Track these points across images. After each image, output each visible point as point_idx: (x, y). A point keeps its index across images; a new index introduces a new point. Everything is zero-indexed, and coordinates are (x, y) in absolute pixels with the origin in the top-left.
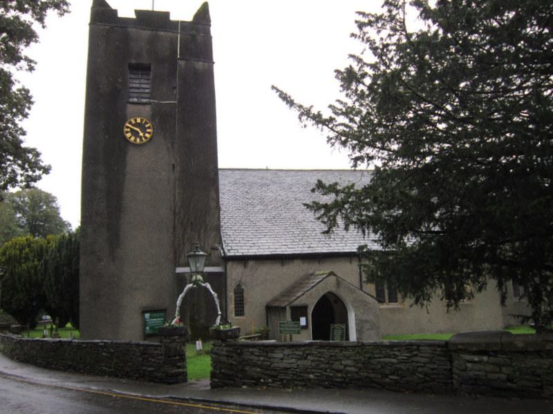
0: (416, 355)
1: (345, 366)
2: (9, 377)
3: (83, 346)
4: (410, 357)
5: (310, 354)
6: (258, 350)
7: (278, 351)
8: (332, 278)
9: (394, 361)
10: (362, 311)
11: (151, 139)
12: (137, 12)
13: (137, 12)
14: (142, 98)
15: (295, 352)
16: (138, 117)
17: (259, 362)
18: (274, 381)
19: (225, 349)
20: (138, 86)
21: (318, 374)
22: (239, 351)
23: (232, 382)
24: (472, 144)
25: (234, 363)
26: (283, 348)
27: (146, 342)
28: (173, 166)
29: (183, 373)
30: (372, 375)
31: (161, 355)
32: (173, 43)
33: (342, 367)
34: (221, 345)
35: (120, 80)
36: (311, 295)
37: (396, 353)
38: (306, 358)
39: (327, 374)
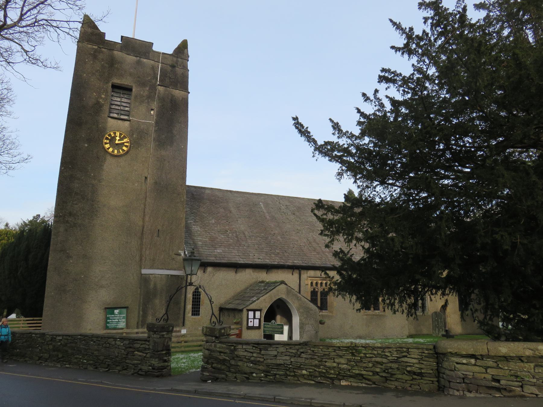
0: (406, 356)
1: (338, 364)
2: (400, 380)
3: (58, 338)
4: (400, 358)
5: (303, 353)
6: (251, 348)
8: (283, 286)
9: (385, 360)
10: (305, 316)
11: (127, 152)
14: (122, 114)
17: (252, 359)
18: (266, 376)
19: (219, 345)
20: (119, 103)
21: (311, 370)
23: (223, 376)
25: (227, 358)
26: (277, 346)
29: (168, 366)
30: (364, 373)
31: (149, 349)
32: (154, 69)
33: (335, 365)
34: (214, 342)
35: (103, 96)
36: (265, 300)
37: (386, 354)
38: (299, 356)
39: (320, 370)
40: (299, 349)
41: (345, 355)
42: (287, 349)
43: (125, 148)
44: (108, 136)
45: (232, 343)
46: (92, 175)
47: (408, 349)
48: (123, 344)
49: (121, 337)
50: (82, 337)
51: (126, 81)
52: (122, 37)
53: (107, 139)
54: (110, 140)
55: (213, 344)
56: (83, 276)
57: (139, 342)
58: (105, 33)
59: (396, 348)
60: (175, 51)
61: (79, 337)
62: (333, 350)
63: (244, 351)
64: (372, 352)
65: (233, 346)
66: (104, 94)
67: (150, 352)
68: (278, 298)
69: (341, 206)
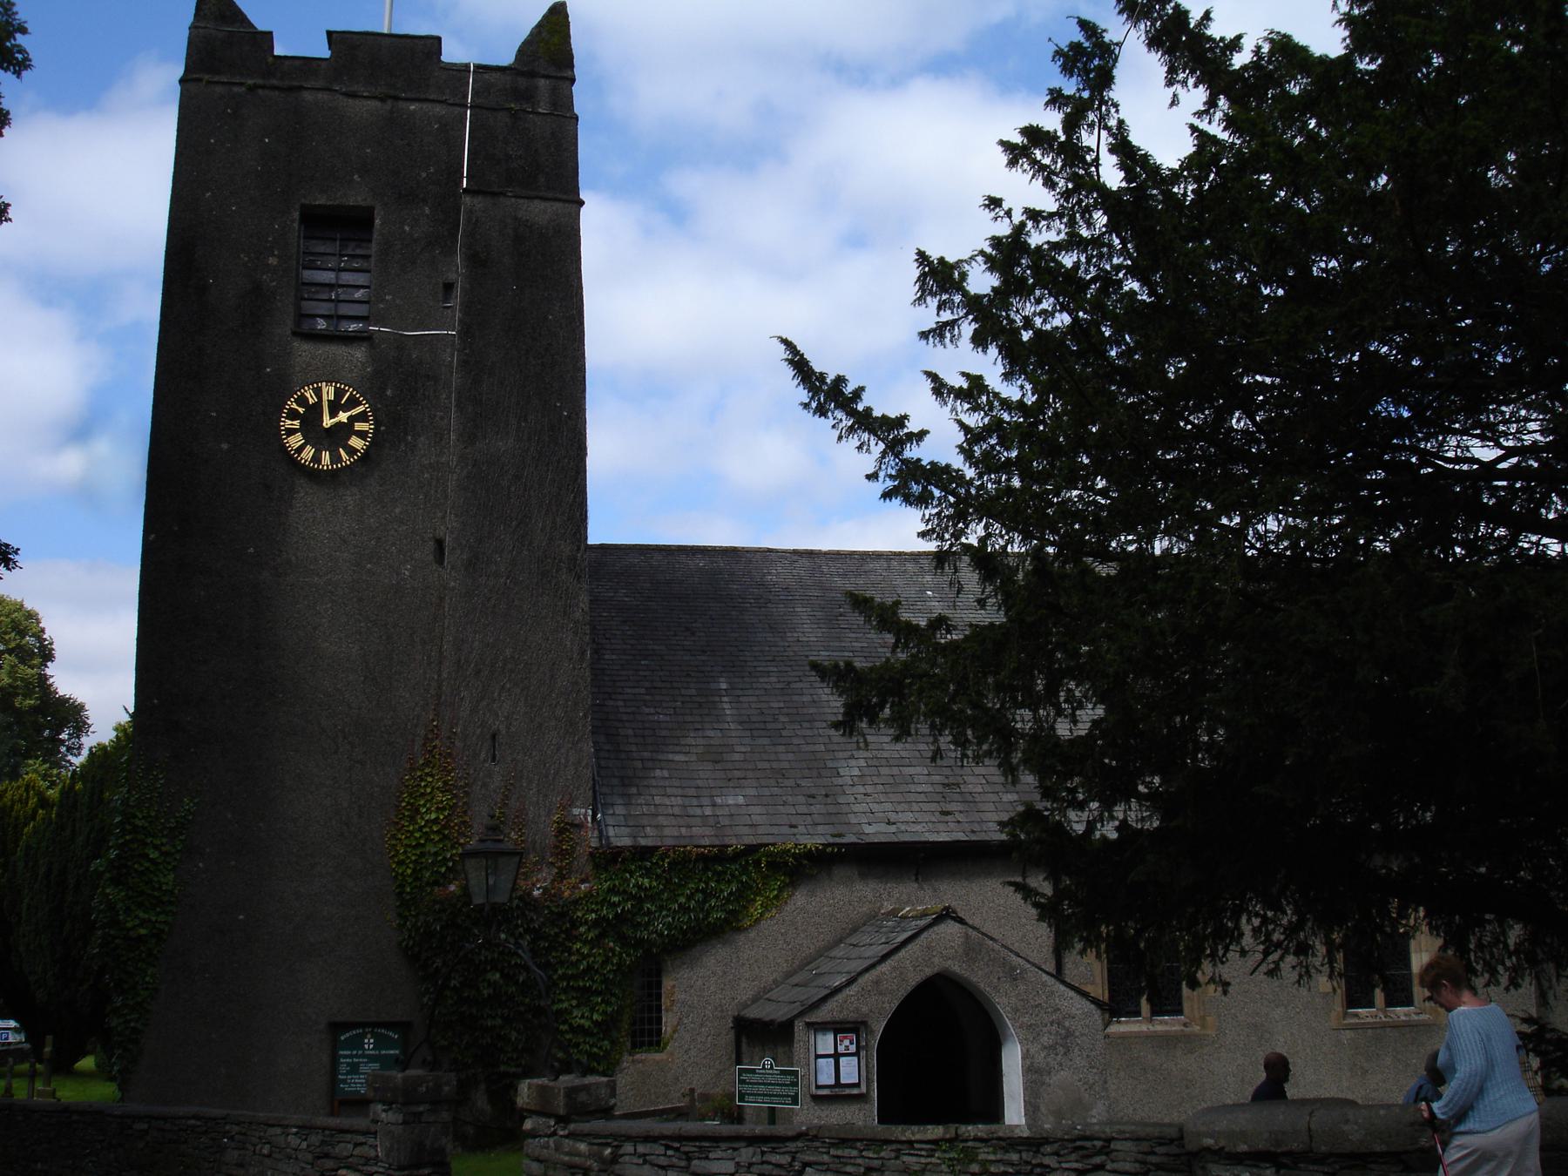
6: (661, 1150)
7: (719, 1154)
8: (950, 929)
12: (335, 38)
13: (335, 38)
15: (767, 1157)
16: (329, 382)
22: (608, 1151)
24: (1051, 643)
26: (736, 1145)
27: (333, 1122)
28: (440, 544)
34: (554, 1134)
35: (272, 261)
36: (877, 982)
37: (1046, 1161)
40: (796, 1152)
41: (929, 1167)
42: (763, 1153)
43: (355, 442)
44: (294, 406)
45: (606, 1137)
46: (252, 550)
47: (1109, 1140)
48: (308, 1146)
49: (301, 1124)
50: (199, 1123)
51: (356, 196)
52: (330, 34)
53: (293, 415)
54: (303, 419)
55: (551, 1140)
56: (241, 917)
57: (349, 1137)
58: (271, 33)
59: (1074, 1141)
60: (521, 52)
61: (192, 1122)
62: (893, 1155)
63: (641, 1161)
64: (1005, 1157)
65: (608, 1145)
66: (276, 253)
67: (381, 1170)
68: (929, 972)
69: (872, 599)
